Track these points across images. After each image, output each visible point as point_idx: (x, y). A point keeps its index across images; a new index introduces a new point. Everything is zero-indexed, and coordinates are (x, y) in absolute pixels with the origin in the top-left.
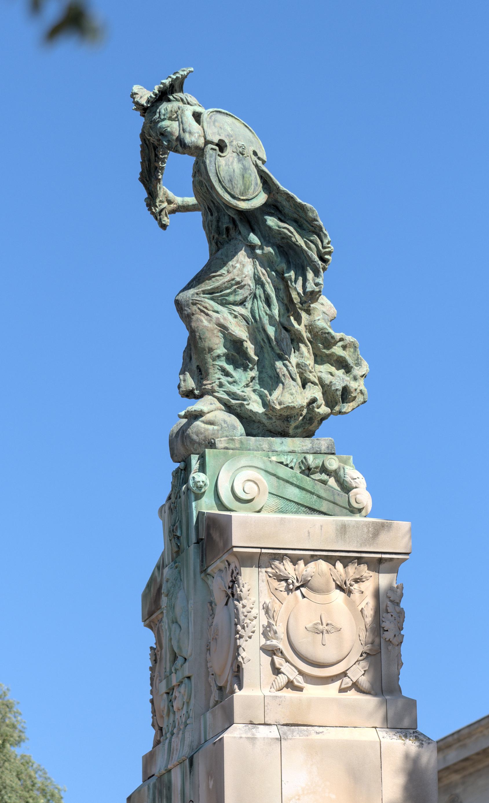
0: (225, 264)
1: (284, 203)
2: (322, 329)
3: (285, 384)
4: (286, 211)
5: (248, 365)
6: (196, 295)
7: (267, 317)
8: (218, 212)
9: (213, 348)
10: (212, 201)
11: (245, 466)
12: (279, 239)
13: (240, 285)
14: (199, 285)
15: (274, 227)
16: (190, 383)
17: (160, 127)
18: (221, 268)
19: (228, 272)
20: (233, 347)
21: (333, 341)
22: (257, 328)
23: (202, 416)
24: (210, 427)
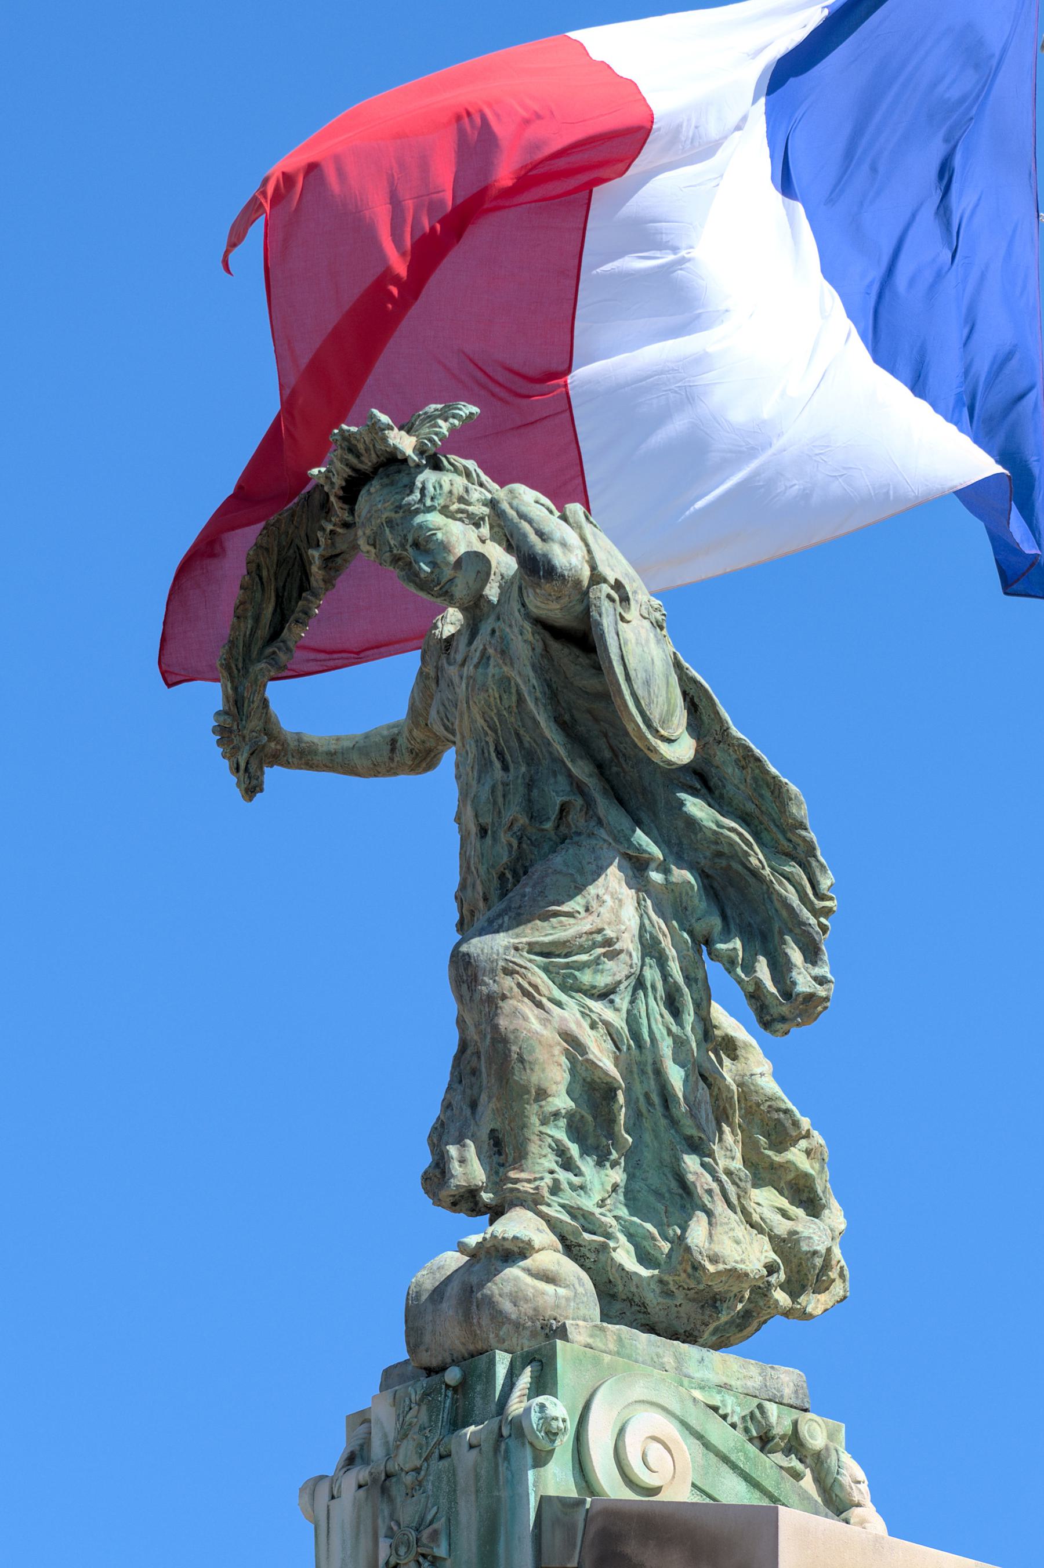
0: (579, 889)
1: (730, 771)
2: (771, 1099)
3: (716, 1213)
4: (730, 790)
5: (610, 1153)
6: (513, 951)
7: (669, 1041)
8: (528, 764)
9: (549, 1092)
10: (518, 735)
11: (643, 1402)
12: (708, 854)
13: (610, 948)
14: (518, 926)
15: (705, 823)
16: (469, 1168)
17: (420, 526)
18: (571, 897)
19: (587, 910)
20: (586, 1097)
21: (794, 1134)
22: (638, 1063)
23: (525, 1257)
24: (550, 1288)
